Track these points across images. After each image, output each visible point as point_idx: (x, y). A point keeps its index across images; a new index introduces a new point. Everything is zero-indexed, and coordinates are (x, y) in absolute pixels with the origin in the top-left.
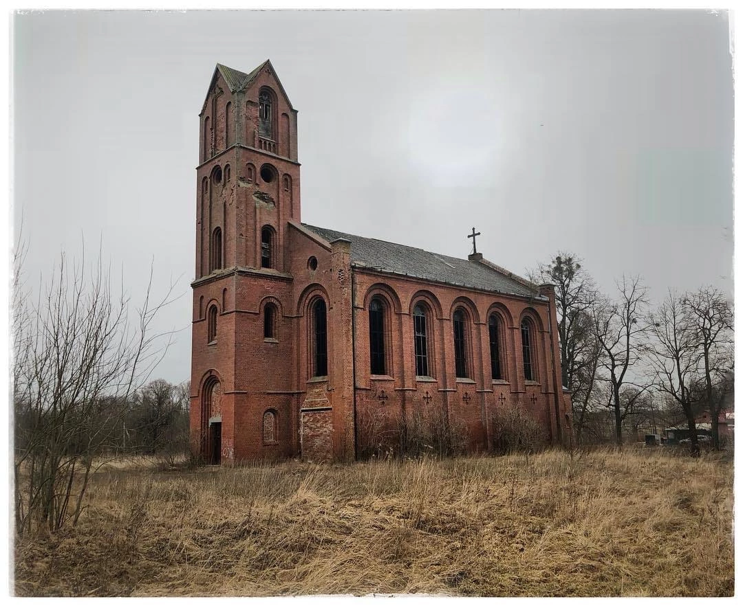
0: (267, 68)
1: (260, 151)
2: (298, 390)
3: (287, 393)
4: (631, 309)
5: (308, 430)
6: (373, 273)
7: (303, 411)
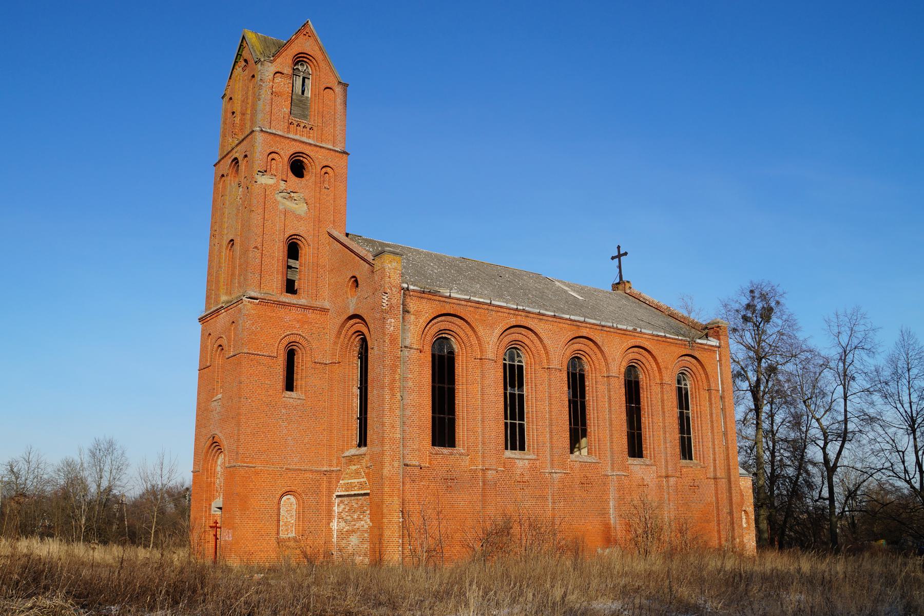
1: (291, 136)
2: (330, 466)
4: (848, 361)
5: (343, 524)
7: (338, 496)
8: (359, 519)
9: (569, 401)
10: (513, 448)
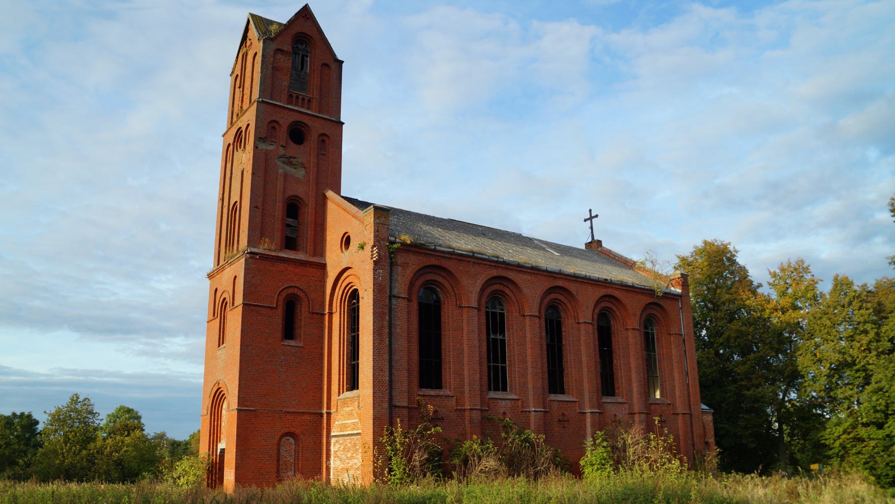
0: (305, 14)
3: (313, 414)
5: (338, 462)
6: (423, 251)
8: (352, 457)
9: (547, 345)
10: (496, 389)
